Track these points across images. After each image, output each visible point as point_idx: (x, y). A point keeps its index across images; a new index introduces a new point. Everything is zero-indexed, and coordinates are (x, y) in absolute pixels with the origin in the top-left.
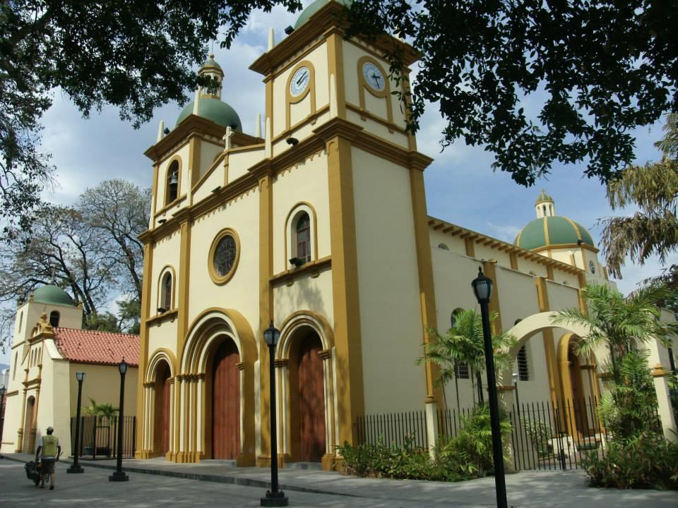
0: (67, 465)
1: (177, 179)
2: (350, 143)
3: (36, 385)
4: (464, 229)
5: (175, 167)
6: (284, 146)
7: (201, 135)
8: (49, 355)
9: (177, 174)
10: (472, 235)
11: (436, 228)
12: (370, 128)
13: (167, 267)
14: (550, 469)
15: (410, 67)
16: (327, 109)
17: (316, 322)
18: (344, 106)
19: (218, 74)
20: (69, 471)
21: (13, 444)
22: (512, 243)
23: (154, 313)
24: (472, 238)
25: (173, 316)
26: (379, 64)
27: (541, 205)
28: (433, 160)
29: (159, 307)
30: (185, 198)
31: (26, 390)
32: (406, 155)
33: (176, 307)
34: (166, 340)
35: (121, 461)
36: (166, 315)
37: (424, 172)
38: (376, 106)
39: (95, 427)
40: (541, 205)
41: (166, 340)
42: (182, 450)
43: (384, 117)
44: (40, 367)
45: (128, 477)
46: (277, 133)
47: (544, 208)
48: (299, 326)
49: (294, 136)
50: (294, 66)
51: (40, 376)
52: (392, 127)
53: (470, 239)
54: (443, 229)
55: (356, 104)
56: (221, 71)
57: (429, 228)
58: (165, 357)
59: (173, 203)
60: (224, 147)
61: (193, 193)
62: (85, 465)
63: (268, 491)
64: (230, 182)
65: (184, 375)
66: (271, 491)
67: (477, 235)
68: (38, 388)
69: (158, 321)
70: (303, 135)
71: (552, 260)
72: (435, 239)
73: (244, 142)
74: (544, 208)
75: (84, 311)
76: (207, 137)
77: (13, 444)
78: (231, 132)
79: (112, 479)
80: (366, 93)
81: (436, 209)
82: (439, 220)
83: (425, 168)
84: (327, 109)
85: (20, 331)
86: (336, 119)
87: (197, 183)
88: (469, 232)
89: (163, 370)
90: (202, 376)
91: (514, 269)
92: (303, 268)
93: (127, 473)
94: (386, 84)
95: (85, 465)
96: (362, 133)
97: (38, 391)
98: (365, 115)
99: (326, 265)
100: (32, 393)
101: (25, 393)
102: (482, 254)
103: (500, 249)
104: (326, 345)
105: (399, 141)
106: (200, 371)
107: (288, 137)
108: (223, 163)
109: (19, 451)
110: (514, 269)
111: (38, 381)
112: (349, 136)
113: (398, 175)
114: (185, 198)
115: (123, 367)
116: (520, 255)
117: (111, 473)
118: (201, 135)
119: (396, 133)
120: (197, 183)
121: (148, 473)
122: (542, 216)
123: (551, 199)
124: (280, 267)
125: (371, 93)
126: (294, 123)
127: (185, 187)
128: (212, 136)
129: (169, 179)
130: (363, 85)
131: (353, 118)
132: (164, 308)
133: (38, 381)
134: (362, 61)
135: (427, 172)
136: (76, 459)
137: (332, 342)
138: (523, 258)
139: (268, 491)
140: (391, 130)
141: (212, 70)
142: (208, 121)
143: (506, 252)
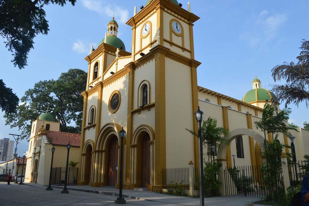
0: (46, 187)
1: (97, 69)
2: (165, 56)
3: (38, 154)
4: (217, 93)
5: (97, 64)
6: (139, 57)
7: (107, 52)
8: (44, 142)
9: (97, 68)
10: (220, 95)
11: (200, 91)
12: (174, 49)
13: (92, 106)
14: (246, 195)
15: (193, 23)
16: (156, 41)
17: (148, 129)
18: (163, 40)
19: (115, 25)
20: (47, 189)
21: (29, 179)
22: (241, 100)
23: (87, 125)
24: (220, 97)
25: (94, 126)
26: (179, 22)
27: (255, 83)
28: (201, 63)
29: (89, 122)
30: (100, 77)
31: (34, 156)
32: (189, 61)
33: (96, 122)
34: (91, 135)
35: (66, 187)
36: (92, 125)
37: (197, 68)
38: (177, 40)
39: (61, 172)
40: (255, 83)
41: (91, 135)
42: (95, 182)
43: (181, 45)
44: (40, 147)
45: (53, 189)
46: (136, 51)
47: (256, 85)
48: (140, 132)
49: (143, 52)
50: (144, 23)
51: (40, 151)
52: (184, 49)
53: (220, 97)
54: (203, 91)
55: (168, 39)
56: (117, 25)
57: (196, 90)
58: (91, 143)
59: (96, 80)
60: (116, 56)
61: (103, 76)
62: (53, 187)
63: (118, 197)
64: (118, 71)
65: (97, 150)
66: (119, 197)
67: (222, 95)
68: (39, 155)
69: (89, 128)
70: (146, 52)
71: (259, 108)
72: (202, 97)
73: (124, 53)
74: (256, 85)
75: (61, 124)
76: (110, 52)
77: (29, 179)
78: (119, 51)
79: (62, 192)
80: (173, 33)
81: (201, 83)
82: (206, 89)
83: (197, 66)
84: (156, 41)
85: (33, 132)
86: (159, 45)
87: (105, 70)
88: (219, 94)
89: (89, 148)
90: (104, 151)
91: (239, 111)
92: (145, 107)
93: (68, 190)
94: (182, 31)
95: (53, 187)
96: (170, 51)
97: (39, 157)
98: (172, 44)
99: (153, 105)
100: (37, 158)
101: (34, 158)
102: (225, 103)
103: (233, 102)
104: (151, 139)
105: (187, 55)
106: (104, 149)
107: (141, 53)
108: (115, 63)
109: (31, 182)
110: (239, 111)
111: (39, 152)
112: (164, 53)
113: (186, 69)
114: (100, 77)
115: (69, 147)
116: (242, 105)
117: (62, 190)
118: (107, 52)
119: (186, 52)
120: (105, 70)
121: (79, 191)
122: (255, 88)
123: (259, 81)
124: (136, 107)
125: (176, 35)
126: (143, 47)
127: (100, 73)
128: (112, 52)
129: (94, 70)
130: (172, 31)
131: (166, 45)
132: (91, 123)
133: (39, 152)
134: (172, 21)
135: (199, 69)
136: (50, 184)
137: (154, 138)
138: (243, 106)
139: (118, 197)
140: (183, 50)
141: (113, 24)
142: (108, 45)
143: (236, 103)
